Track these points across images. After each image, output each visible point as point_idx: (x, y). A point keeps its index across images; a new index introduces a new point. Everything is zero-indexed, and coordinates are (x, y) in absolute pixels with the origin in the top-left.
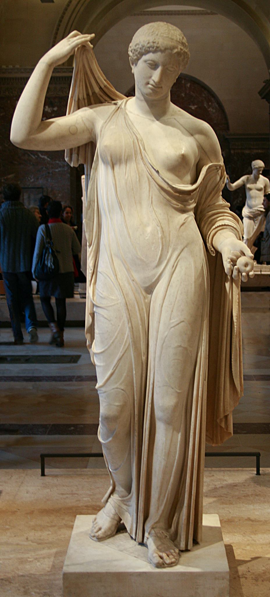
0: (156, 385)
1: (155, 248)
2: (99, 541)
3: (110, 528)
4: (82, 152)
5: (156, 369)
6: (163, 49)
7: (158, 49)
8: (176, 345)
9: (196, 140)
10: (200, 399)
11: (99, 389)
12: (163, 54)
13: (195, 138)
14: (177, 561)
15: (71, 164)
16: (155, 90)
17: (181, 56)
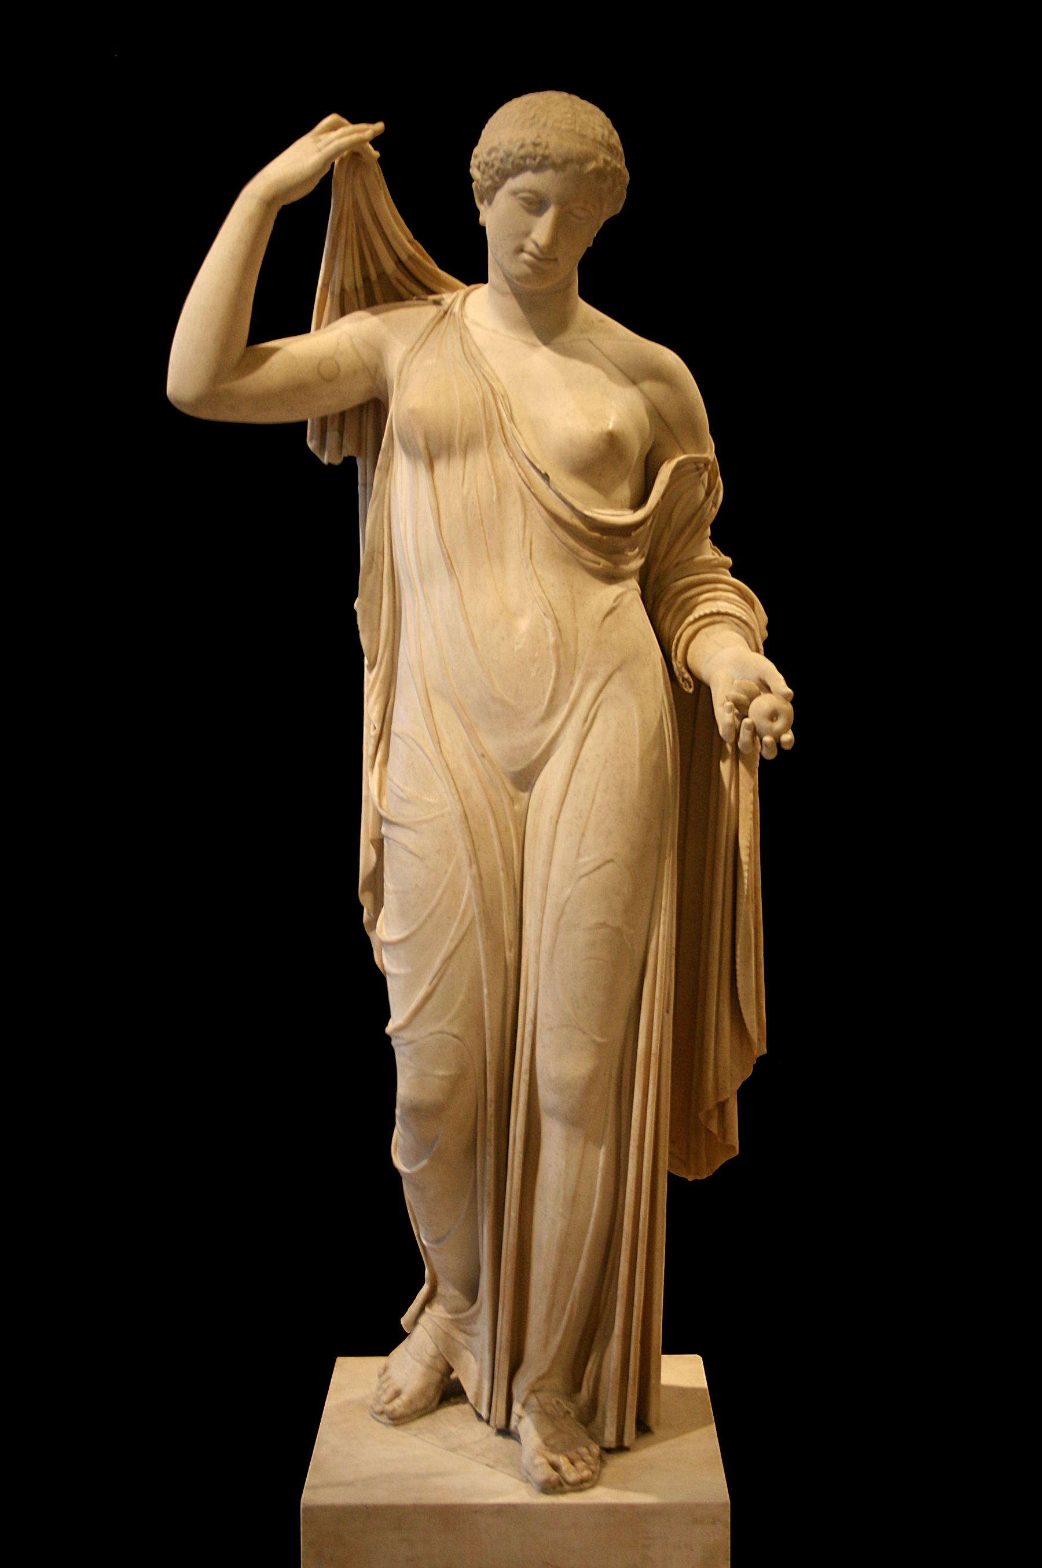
2: (396, 1425)
3: (422, 1393)
4: (350, 427)
6: (559, 161)
7: (547, 162)
8: (593, 921)
9: (645, 395)
12: (561, 175)
13: (641, 391)
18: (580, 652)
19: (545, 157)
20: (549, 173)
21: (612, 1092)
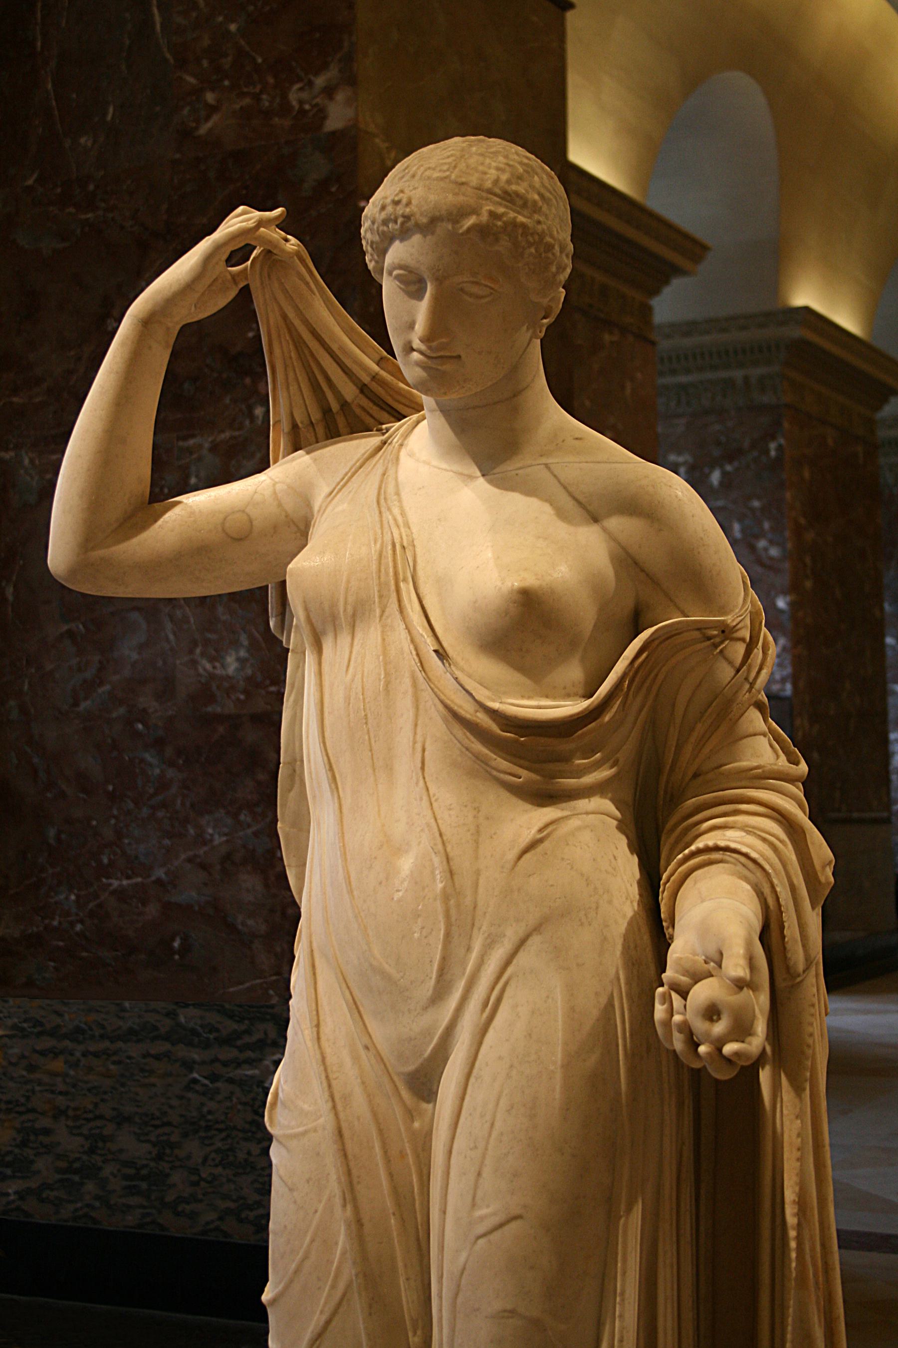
6: (424, 220)
7: (410, 224)
9: (610, 536)
13: (605, 530)
15: (283, 638)
16: (431, 368)
18: (480, 903)
19: (407, 218)
20: (417, 238)
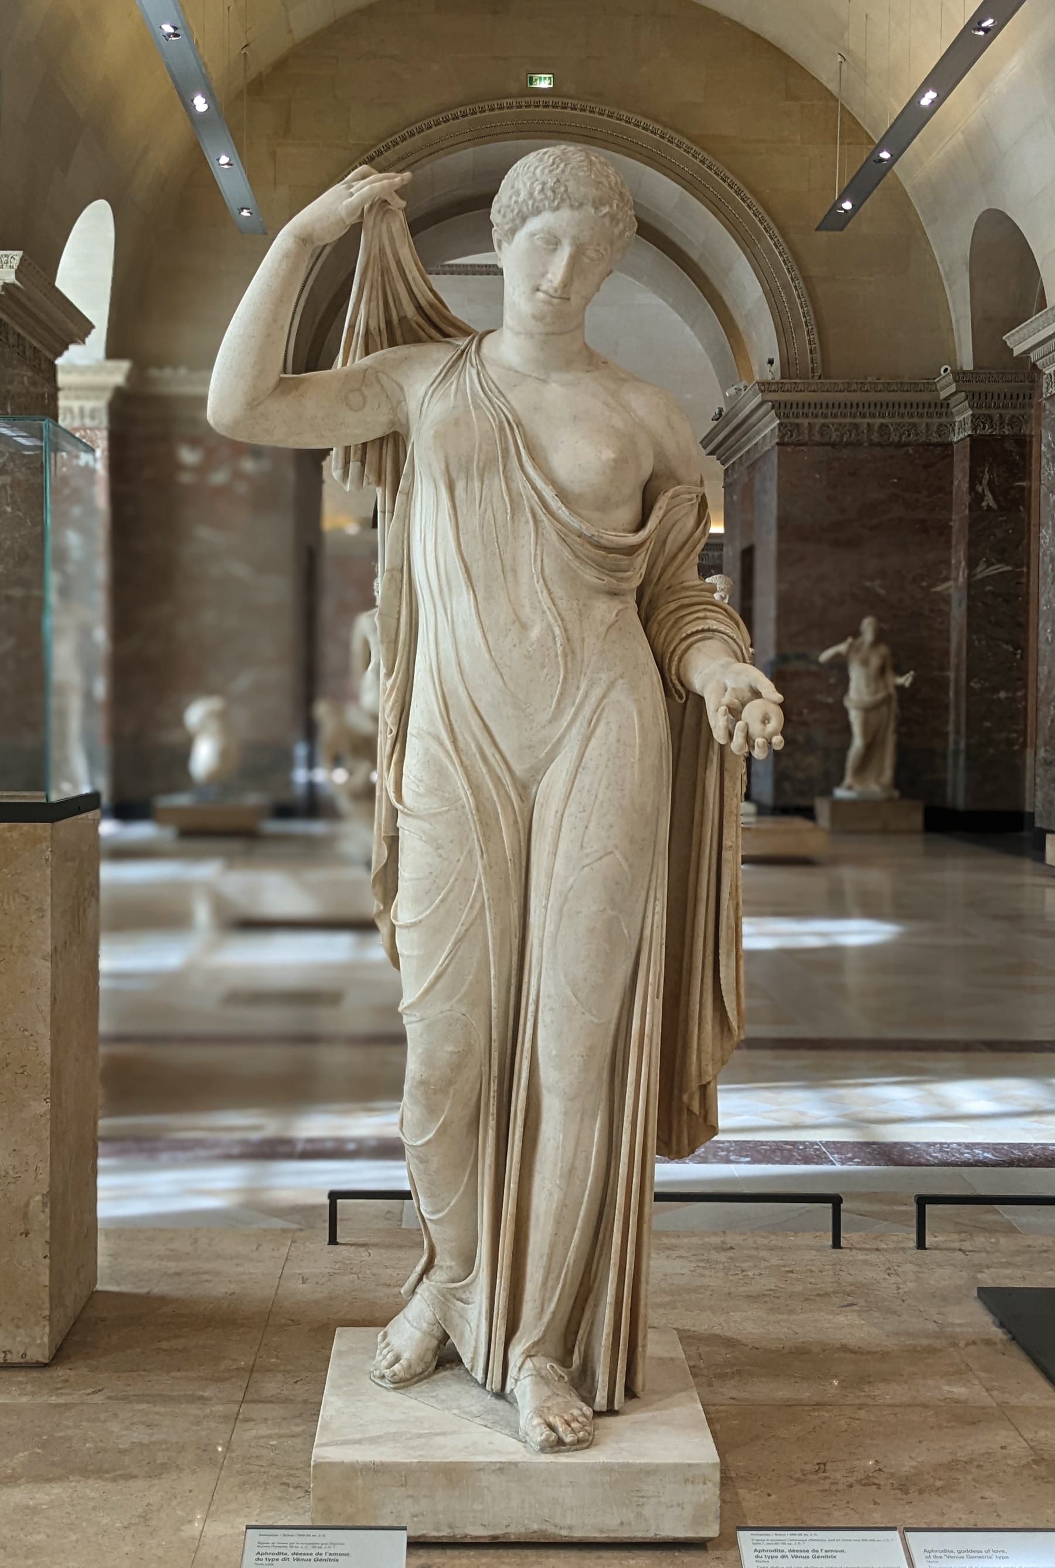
0: (545, 1006)
1: (548, 678)
4: (371, 455)
5: (544, 965)
10: (646, 1040)
11: (408, 1012)
14: (591, 1438)
17: (617, 224)
21: (605, 1075)
